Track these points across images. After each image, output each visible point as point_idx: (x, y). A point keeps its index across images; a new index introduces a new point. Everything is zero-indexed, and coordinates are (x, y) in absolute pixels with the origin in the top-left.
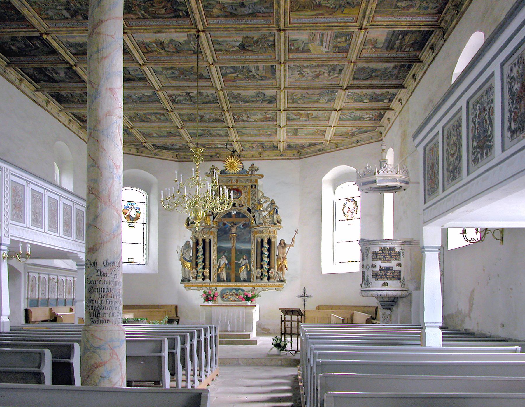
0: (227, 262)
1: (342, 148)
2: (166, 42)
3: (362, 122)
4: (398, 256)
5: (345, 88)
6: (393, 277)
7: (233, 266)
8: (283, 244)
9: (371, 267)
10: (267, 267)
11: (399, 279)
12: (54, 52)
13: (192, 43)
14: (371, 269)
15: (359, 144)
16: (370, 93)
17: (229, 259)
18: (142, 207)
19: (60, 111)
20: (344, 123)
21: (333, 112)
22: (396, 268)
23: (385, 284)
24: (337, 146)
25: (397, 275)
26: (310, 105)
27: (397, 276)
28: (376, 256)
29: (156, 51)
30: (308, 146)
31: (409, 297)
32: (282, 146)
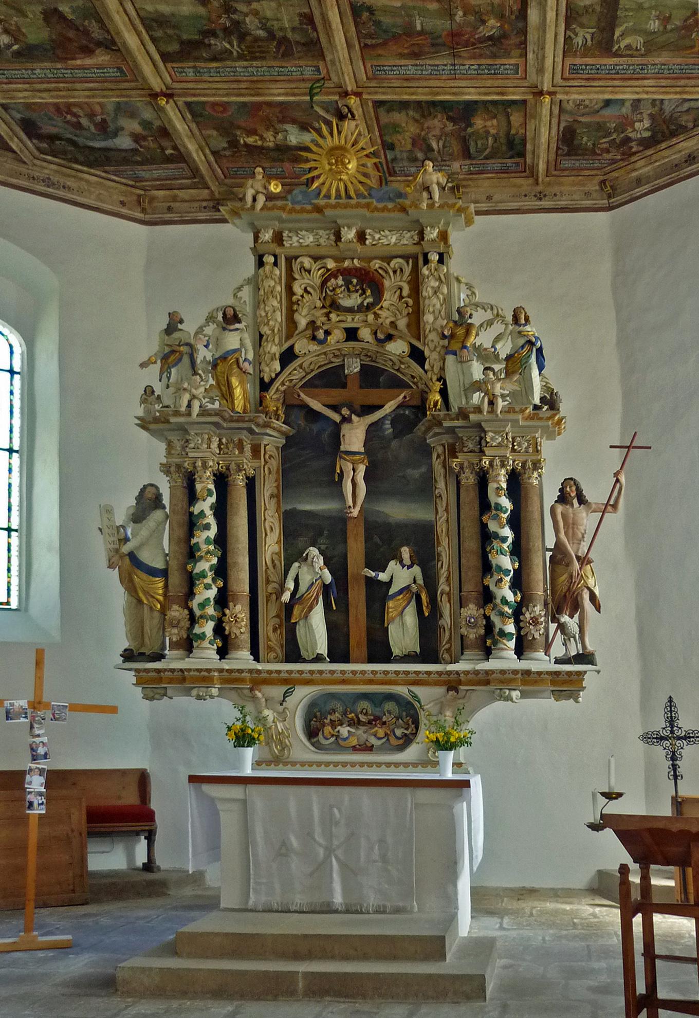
0: (328, 577)
17: (337, 564)
32: (543, 135)
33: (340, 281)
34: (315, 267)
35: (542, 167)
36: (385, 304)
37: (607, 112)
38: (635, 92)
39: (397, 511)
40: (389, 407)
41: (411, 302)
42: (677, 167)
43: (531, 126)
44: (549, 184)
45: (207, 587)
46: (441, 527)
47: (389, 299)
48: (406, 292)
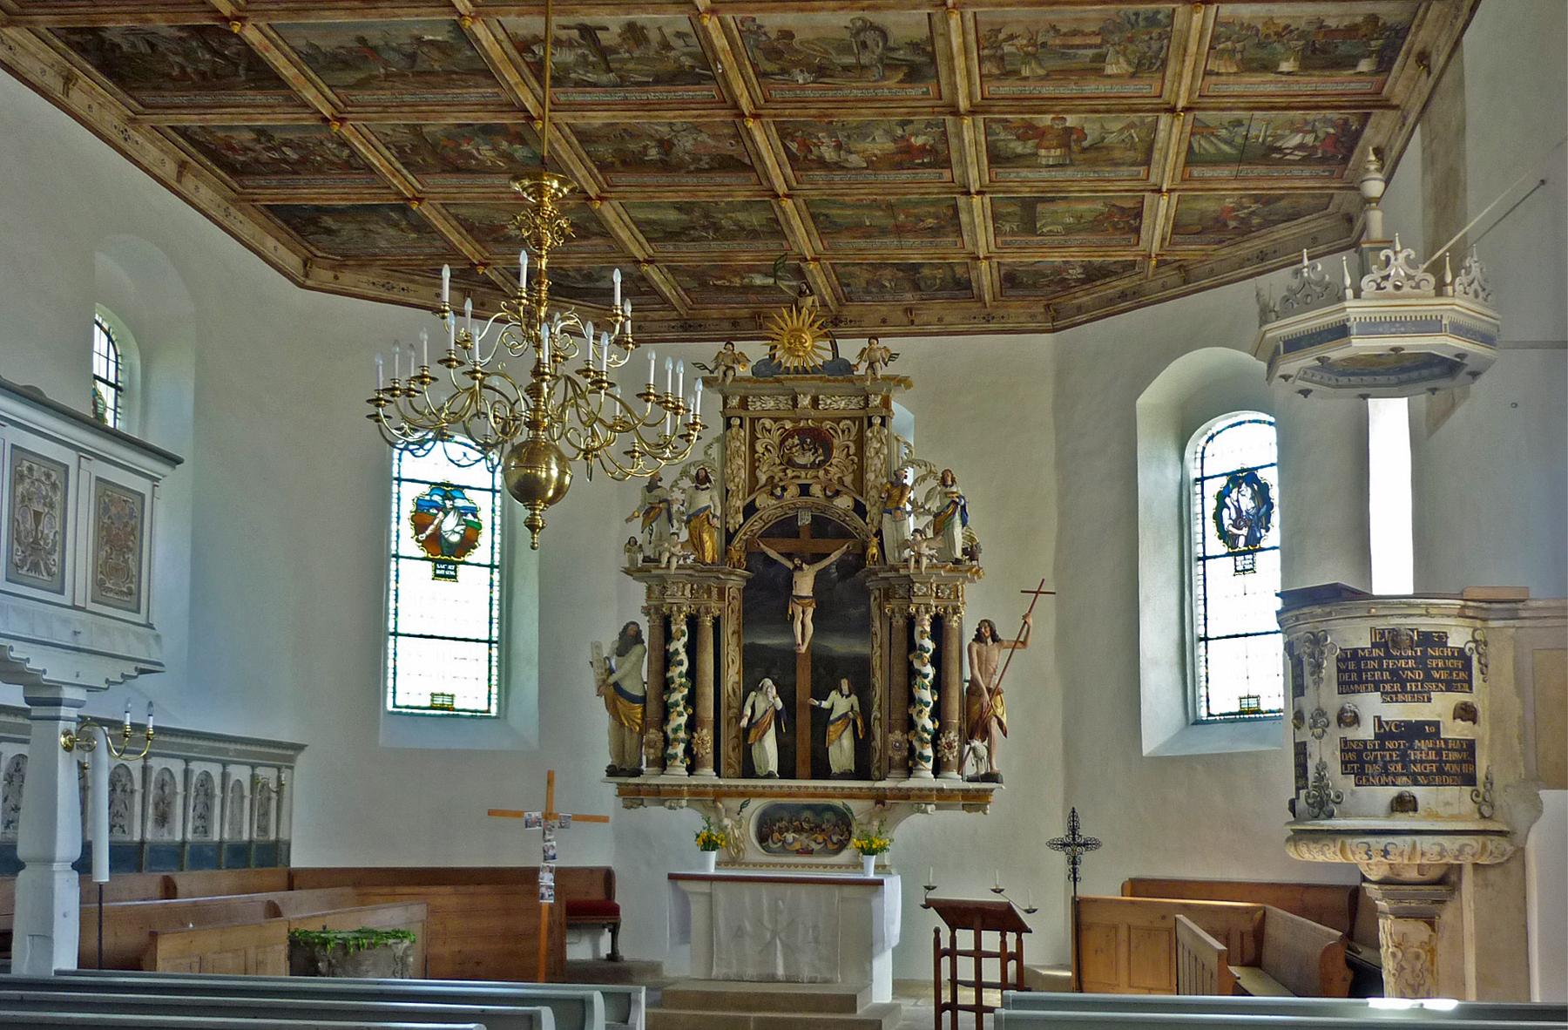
0: (779, 705)
1: (1205, 282)
3: (1275, 171)
4: (1459, 671)
6: (1441, 772)
7: (804, 720)
8: (986, 634)
9: (1334, 720)
10: (929, 725)
11: (1470, 780)
14: (1336, 734)
15: (1269, 264)
16: (1302, 25)
18: (483, 501)
20: (1208, 172)
21: (1165, 119)
22: (1455, 730)
23: (1403, 804)
24: (1187, 279)
25: (1460, 762)
26: (1069, 89)
27: (1458, 766)
28: (1359, 672)
30: (1083, 282)
31: (1514, 865)
32: (986, 277)
33: (796, 441)
34: (775, 426)
36: (834, 461)
39: (840, 646)
40: (835, 556)
42: (1111, 301)
45: (680, 714)
46: (876, 662)
48: (852, 451)
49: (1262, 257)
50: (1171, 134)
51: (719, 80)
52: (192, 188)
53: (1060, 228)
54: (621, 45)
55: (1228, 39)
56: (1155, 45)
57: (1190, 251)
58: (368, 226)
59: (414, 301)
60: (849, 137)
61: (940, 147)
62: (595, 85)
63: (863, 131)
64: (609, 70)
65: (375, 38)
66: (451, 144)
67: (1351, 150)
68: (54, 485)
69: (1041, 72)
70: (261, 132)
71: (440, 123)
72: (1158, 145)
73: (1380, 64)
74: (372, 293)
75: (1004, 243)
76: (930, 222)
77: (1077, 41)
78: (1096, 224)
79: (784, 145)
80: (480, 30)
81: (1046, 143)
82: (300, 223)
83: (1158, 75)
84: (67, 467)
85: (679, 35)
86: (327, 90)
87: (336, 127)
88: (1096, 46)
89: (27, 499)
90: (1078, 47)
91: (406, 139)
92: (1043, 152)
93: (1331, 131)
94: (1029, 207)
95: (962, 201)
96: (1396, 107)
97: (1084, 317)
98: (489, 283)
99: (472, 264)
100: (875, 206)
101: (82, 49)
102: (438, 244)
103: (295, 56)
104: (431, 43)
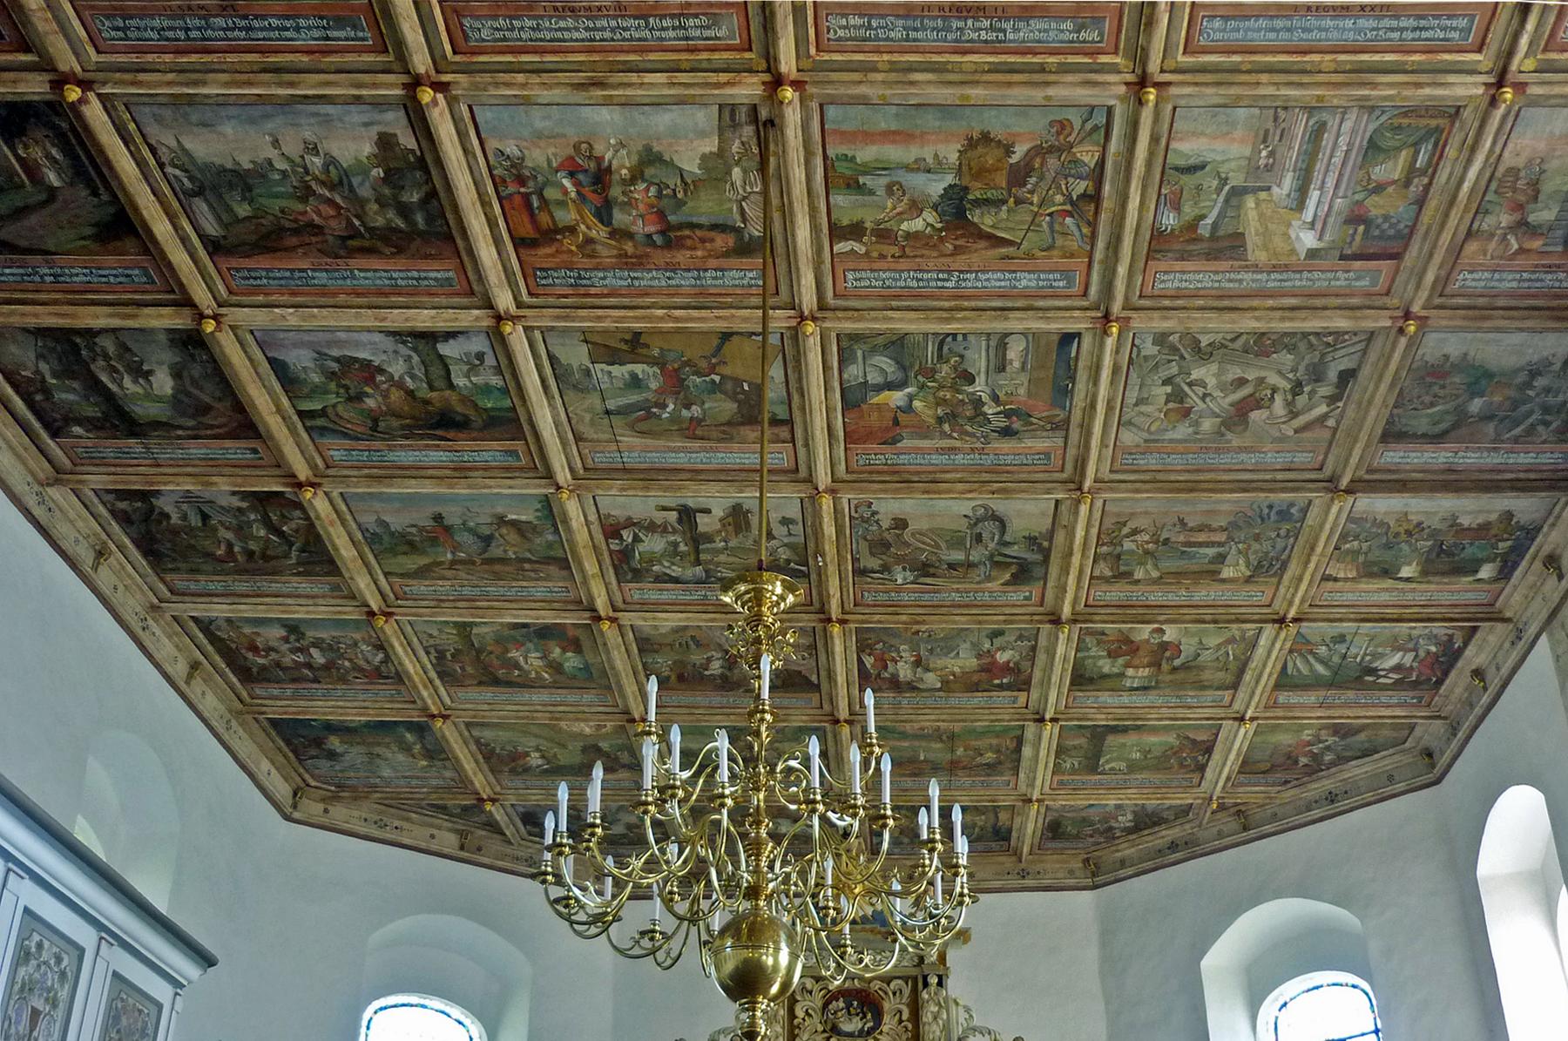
1: (1267, 828)
2: (622, 164)
5: (1344, 482)
12: (120, 226)
13: (736, 172)
19: (153, 608)
21: (1269, 630)
24: (1246, 824)
29: (572, 230)
30: (1129, 831)
32: (1030, 826)
33: (841, 1004)
34: (817, 987)
35: (1026, 850)
36: (885, 1028)
37: (1091, 810)
38: (1116, 799)
41: (910, 1026)
42: (1160, 852)
43: (1017, 820)
44: (1032, 862)
47: (888, 1023)
48: (905, 1017)
49: (1332, 798)
50: (1271, 647)
51: (813, 576)
52: (199, 692)
53: (1123, 765)
54: (719, 532)
55: (1356, 537)
56: (1280, 543)
57: (1252, 794)
58: (378, 750)
59: (407, 841)
60: (931, 651)
61: (1025, 665)
62: (676, 580)
63: (948, 644)
64: (698, 562)
65: (453, 517)
66: (498, 650)
67: (1446, 674)
68: (63, 974)
69: (1155, 574)
70: (293, 628)
71: (492, 621)
72: (1252, 665)
73: (1501, 571)
74: (363, 830)
75: (1061, 783)
76: (990, 756)
77: (1202, 537)
78: (1159, 762)
79: (860, 661)
80: (572, 508)
81: (1136, 662)
82: (301, 742)
83: (1274, 580)
84: (82, 951)
85: (786, 521)
86: (381, 578)
87: (381, 621)
88: (1220, 544)
89: (28, 988)
90: (1201, 545)
91: (450, 640)
92: (1130, 672)
93: (1433, 649)
94: (1098, 735)
95: (1031, 729)
96: (1508, 620)
97: (1130, 871)
98: (493, 827)
99: (481, 800)
100: (937, 735)
101: (124, 519)
102: (448, 774)
103: (359, 536)
104: (514, 523)
